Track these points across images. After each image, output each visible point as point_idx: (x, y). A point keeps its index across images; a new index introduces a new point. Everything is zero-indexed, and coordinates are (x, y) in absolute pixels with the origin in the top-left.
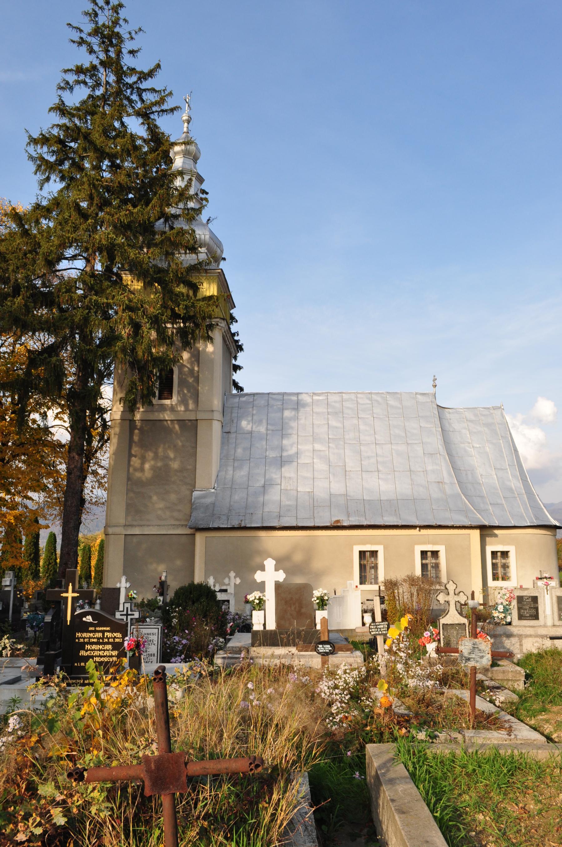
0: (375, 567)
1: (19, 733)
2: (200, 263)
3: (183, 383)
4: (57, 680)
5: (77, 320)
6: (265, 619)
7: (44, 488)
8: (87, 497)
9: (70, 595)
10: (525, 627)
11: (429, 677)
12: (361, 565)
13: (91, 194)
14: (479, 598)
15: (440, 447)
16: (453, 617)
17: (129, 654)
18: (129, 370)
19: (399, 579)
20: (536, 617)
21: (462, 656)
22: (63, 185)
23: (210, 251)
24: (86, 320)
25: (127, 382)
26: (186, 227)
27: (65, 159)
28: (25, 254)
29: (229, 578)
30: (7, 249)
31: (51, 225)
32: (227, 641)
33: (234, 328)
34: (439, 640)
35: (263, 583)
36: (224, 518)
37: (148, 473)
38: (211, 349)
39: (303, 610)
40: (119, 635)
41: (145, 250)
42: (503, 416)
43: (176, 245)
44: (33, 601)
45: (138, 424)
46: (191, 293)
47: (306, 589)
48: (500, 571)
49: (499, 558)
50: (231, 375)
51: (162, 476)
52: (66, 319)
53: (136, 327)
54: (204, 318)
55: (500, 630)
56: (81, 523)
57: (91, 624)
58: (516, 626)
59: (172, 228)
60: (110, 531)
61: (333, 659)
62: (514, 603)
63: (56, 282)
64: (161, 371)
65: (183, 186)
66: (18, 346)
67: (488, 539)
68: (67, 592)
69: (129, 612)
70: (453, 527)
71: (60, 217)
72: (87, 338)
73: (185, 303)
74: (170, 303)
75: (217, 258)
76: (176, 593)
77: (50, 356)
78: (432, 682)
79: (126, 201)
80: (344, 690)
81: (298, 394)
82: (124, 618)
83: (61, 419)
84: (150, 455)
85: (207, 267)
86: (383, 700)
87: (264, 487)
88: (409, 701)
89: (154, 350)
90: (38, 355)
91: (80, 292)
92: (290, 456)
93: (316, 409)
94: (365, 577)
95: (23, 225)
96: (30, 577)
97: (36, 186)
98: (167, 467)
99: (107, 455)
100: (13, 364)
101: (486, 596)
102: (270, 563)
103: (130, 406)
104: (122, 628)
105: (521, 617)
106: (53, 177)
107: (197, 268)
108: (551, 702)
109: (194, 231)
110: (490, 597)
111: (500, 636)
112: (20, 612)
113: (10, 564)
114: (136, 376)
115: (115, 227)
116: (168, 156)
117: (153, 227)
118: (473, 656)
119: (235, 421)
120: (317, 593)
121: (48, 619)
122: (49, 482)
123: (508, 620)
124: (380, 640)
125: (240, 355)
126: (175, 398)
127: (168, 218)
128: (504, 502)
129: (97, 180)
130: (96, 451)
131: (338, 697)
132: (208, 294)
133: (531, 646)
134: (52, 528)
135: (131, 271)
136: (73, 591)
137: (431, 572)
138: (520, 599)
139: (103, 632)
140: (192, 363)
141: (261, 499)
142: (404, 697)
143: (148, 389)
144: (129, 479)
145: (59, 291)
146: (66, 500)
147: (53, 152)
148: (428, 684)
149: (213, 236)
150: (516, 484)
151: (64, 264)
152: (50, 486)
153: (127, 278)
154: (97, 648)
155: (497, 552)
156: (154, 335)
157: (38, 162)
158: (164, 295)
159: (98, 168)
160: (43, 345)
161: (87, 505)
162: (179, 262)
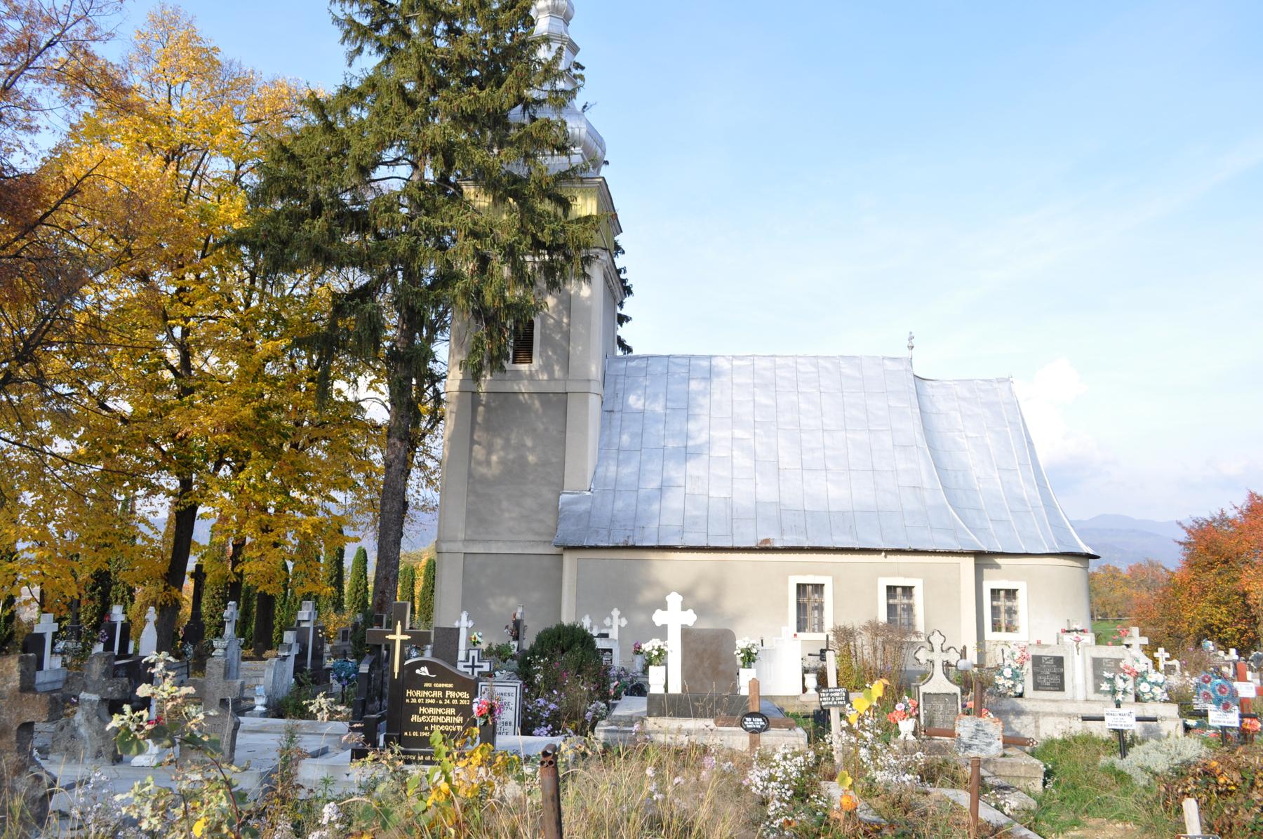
0: (820, 608)
1: (337, 826)
2: (573, 169)
3: (546, 340)
4: (390, 756)
5: (400, 250)
6: (666, 678)
7: (354, 486)
8: (411, 500)
9: (398, 637)
10: (1044, 700)
11: (907, 770)
12: (798, 604)
13: (421, 72)
14: (972, 657)
15: (918, 436)
16: (939, 684)
17: (480, 722)
18: (473, 322)
19: (856, 627)
20: (1061, 687)
21: (960, 741)
22: (381, 58)
23: (587, 151)
24: (413, 251)
25: (469, 339)
26: (554, 118)
27: (384, 22)
28: (329, 158)
29: (612, 618)
30: (304, 151)
31: (365, 115)
32: (610, 708)
33: (620, 262)
34: (918, 716)
35: (665, 627)
36: (604, 532)
37: (494, 470)
38: (587, 292)
39: (722, 667)
40: (465, 695)
41: (496, 151)
42: (1011, 392)
43: (539, 143)
44: (337, 643)
45: (484, 398)
46: (560, 212)
47: (726, 637)
48: (1003, 618)
49: (1002, 599)
50: (614, 332)
51: (515, 472)
52: (385, 249)
53: (484, 261)
54: (578, 248)
55: (1006, 704)
56: (402, 535)
57: (426, 679)
58: (1030, 699)
59: (533, 119)
60: (444, 547)
61: (767, 738)
62: (1028, 665)
63: (370, 196)
64: (517, 322)
65: (550, 59)
66: (317, 287)
67: (986, 572)
68: (394, 633)
69: (476, 663)
70: (934, 553)
71: (377, 105)
72: (413, 276)
73: (552, 226)
74: (530, 226)
75: (596, 161)
76: (539, 638)
77: (363, 301)
78: (911, 777)
79: (469, 82)
80: (783, 783)
81: (711, 357)
82: (470, 670)
83: (376, 389)
84: (499, 442)
85: (583, 175)
86: (845, 801)
87: (661, 489)
88: (878, 803)
89: (507, 294)
90: (347, 299)
91: (404, 211)
92: (700, 446)
93: (737, 380)
94: (805, 621)
95: (326, 117)
96: (331, 609)
97: (344, 61)
98: (522, 462)
99: (439, 441)
100: (310, 312)
101: (981, 655)
102: (674, 600)
103: (474, 372)
104: (471, 687)
105: (1037, 686)
106: (367, 48)
107: (565, 176)
108: (1087, 812)
109: (565, 123)
110: (988, 657)
111: (1006, 712)
112: (321, 657)
113: (307, 590)
114: (483, 330)
115: (454, 118)
116: (527, 15)
117: (506, 117)
118: (976, 742)
119: (620, 395)
120: (741, 643)
121: (364, 668)
122: (358, 477)
123: (1019, 690)
124: (834, 715)
125: (628, 301)
126: (537, 361)
127: (526, 104)
128: (1011, 518)
129: (429, 51)
130: (424, 435)
131: (776, 792)
132: (584, 212)
133: (1051, 729)
134: (363, 541)
135: (475, 180)
136: (403, 633)
137: (902, 616)
138: (1037, 660)
139: (444, 690)
140: (559, 313)
141: (655, 507)
142: (870, 797)
143: (499, 348)
144: (470, 475)
145: (376, 209)
146: (383, 504)
147: (368, 11)
148: (905, 779)
149: (592, 131)
150: (1029, 492)
151: (381, 172)
152: (361, 484)
153: (469, 190)
154: (434, 711)
155: (999, 590)
156: (507, 271)
157: (347, 27)
158: (522, 215)
159: (429, 34)
160: (351, 285)
161: (410, 511)
162: (543, 167)
